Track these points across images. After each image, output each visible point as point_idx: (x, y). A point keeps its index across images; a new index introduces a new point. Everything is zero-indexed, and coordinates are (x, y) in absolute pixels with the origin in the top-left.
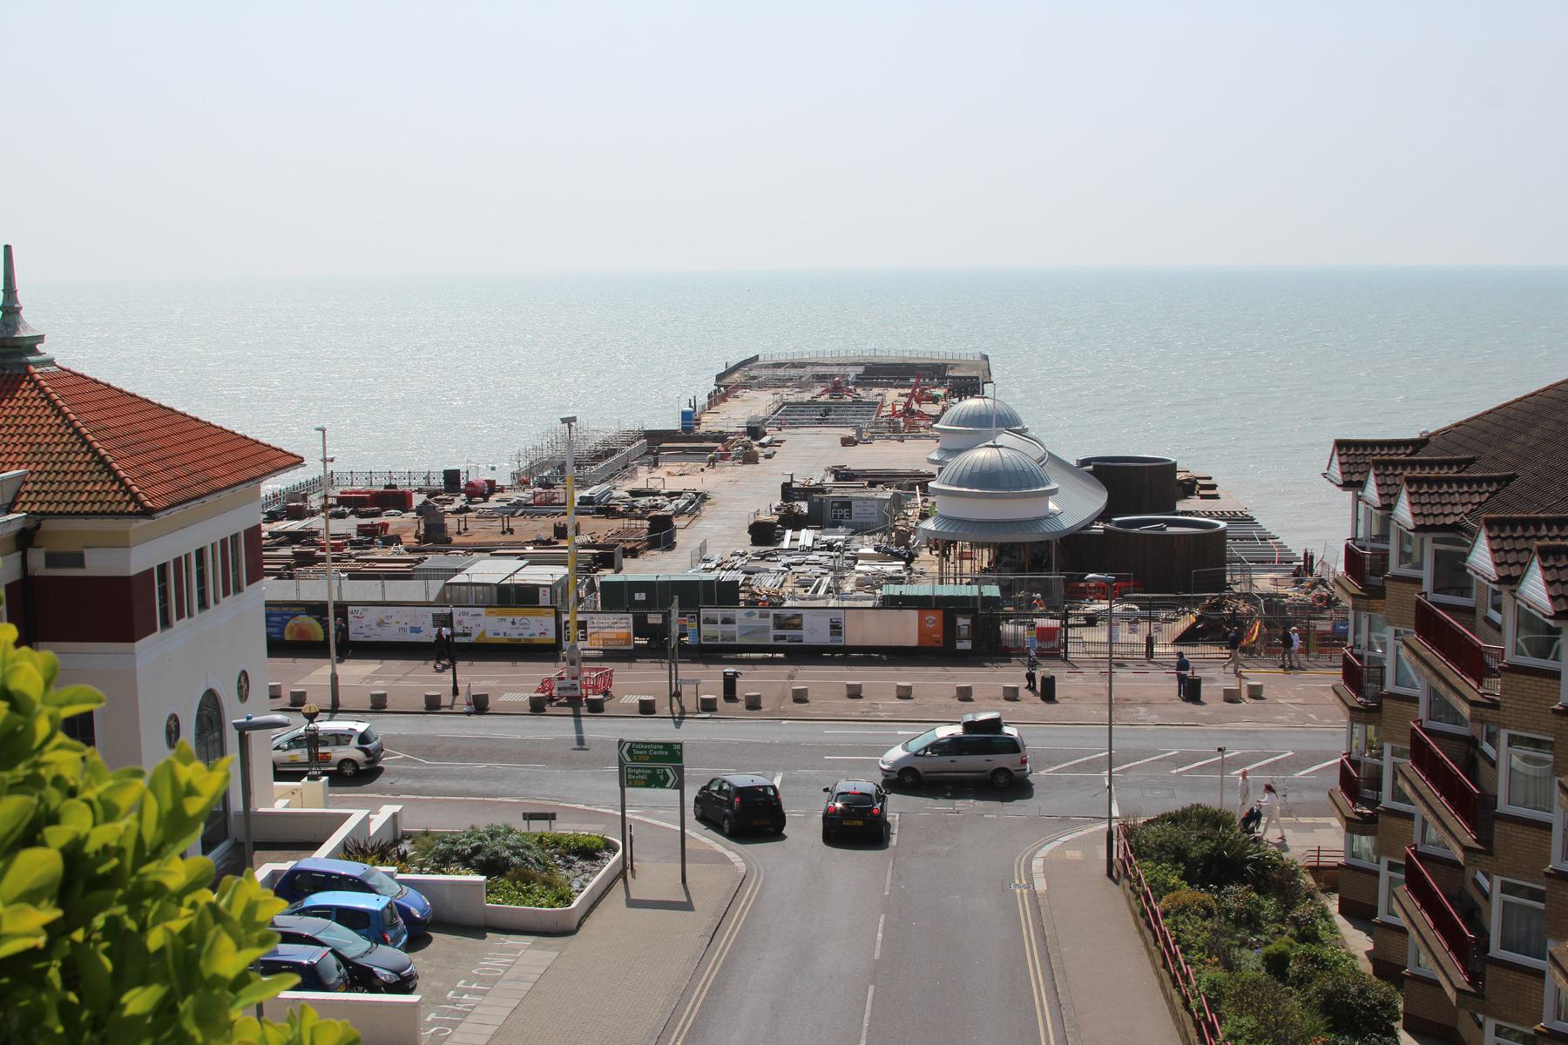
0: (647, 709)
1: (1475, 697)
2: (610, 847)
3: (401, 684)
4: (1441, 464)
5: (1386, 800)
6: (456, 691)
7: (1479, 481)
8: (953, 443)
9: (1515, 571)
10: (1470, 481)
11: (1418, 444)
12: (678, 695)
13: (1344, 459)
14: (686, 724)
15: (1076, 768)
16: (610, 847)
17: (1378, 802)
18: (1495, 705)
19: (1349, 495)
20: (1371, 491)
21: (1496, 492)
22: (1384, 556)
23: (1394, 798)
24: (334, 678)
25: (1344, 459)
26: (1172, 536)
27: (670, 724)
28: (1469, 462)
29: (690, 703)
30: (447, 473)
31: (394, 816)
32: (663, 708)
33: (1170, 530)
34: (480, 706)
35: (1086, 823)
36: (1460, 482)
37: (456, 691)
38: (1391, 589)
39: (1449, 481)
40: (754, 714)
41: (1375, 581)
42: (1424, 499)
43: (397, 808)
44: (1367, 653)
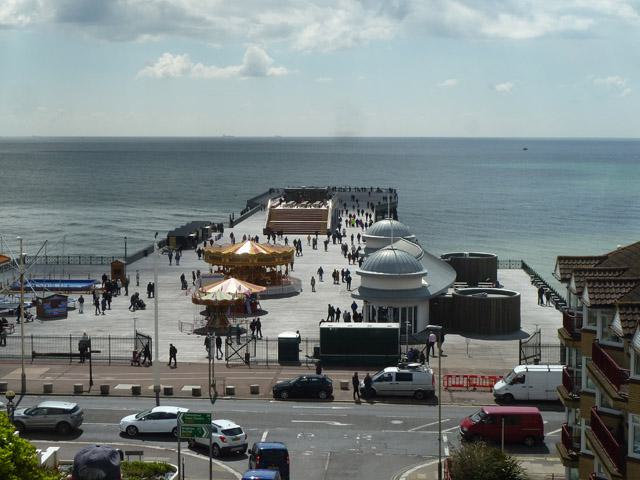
0: (196, 393)
1: (615, 395)
2: (171, 470)
3: (62, 378)
4: (610, 271)
5: (583, 450)
6: (91, 383)
7: (626, 282)
8: (373, 245)
9: (631, 331)
10: (621, 282)
11: (605, 258)
12: (214, 386)
13: (562, 266)
14: (217, 402)
15: (428, 429)
16: (171, 470)
17: (579, 449)
18: (626, 400)
19: (566, 285)
20: (573, 285)
21: (634, 288)
22: (580, 317)
23: (587, 448)
24: (24, 376)
25: (562, 266)
26: (491, 298)
27: (209, 402)
28: (624, 270)
29: (220, 390)
30: (102, 387)
31: (55, 453)
32: (205, 393)
33: (490, 296)
34: (105, 392)
35: (430, 459)
36: (615, 282)
37: (91, 383)
38: (584, 336)
39: (610, 281)
40: (255, 397)
41: (577, 330)
42: (596, 291)
43: (56, 449)
44: (575, 370)
